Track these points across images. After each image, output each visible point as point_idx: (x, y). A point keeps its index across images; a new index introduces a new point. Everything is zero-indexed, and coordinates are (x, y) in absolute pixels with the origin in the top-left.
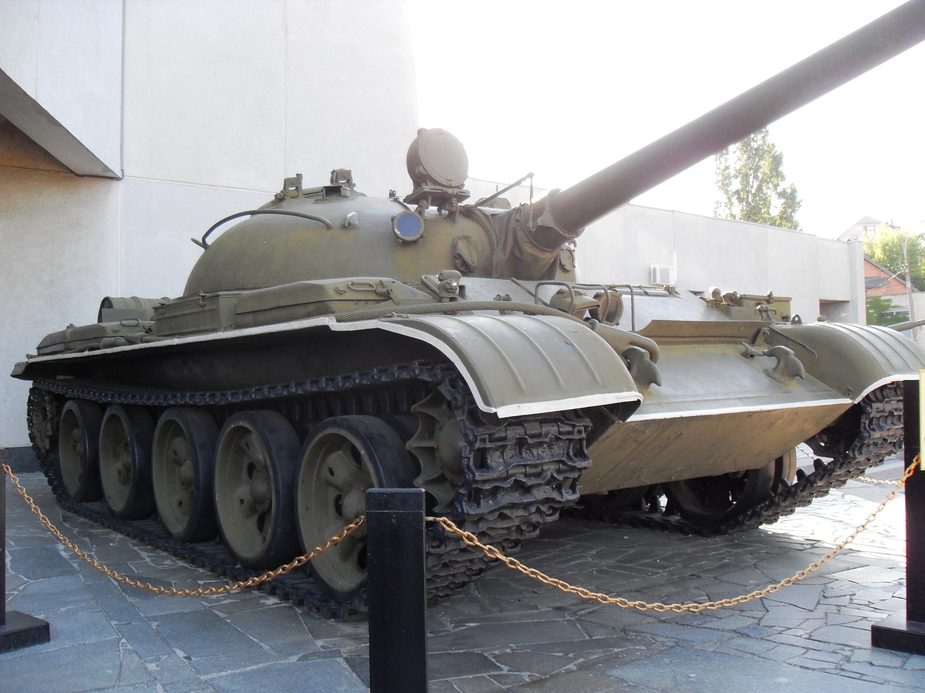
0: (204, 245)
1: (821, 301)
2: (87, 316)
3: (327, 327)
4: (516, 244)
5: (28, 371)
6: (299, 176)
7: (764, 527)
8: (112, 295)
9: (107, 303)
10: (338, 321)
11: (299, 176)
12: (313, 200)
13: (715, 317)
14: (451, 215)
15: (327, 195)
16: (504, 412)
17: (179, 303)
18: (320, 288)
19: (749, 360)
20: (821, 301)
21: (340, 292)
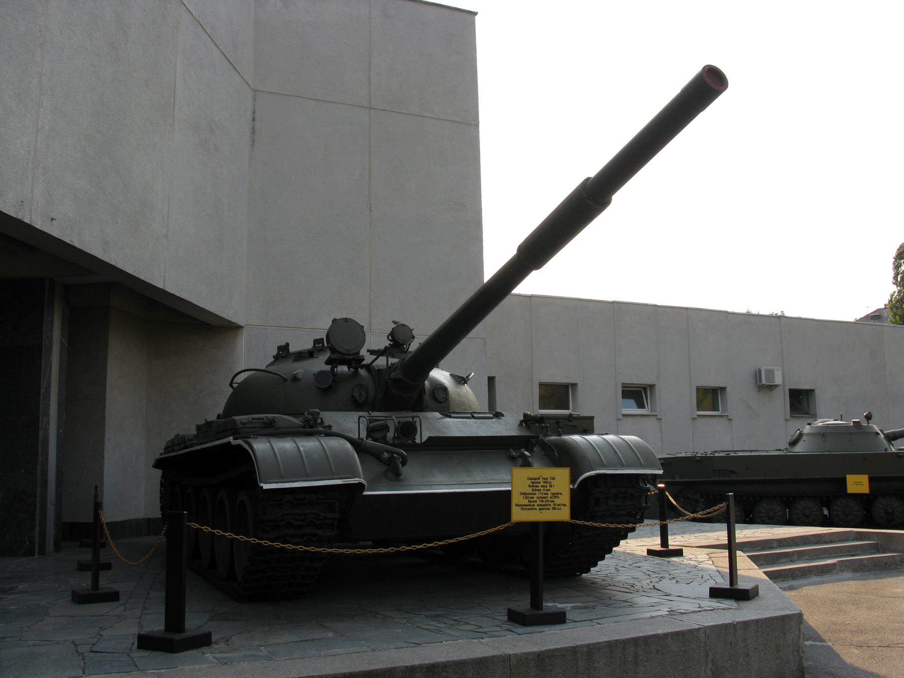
5: (158, 464)
6: (287, 344)
10: (235, 439)
11: (287, 344)
16: (266, 486)
21: (242, 423)
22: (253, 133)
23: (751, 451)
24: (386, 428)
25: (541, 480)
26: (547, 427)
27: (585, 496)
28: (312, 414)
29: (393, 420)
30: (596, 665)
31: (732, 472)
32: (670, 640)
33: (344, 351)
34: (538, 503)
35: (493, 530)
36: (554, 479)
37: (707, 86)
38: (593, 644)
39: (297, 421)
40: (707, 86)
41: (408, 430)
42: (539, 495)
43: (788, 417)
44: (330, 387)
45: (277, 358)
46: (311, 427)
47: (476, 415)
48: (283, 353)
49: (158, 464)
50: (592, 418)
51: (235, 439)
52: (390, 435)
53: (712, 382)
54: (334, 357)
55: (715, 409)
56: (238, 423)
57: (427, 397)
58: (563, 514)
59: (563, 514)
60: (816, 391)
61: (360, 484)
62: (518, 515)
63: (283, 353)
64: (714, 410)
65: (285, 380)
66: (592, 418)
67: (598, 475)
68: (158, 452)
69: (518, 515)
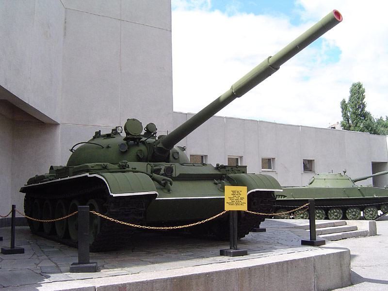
0: (71, 150)
1: (372, 162)
2: (45, 171)
3: (87, 176)
4: (154, 152)
5: (23, 190)
6: (100, 131)
7: (242, 239)
8: (53, 165)
9: (52, 168)
10: (90, 174)
11: (100, 131)
12: (103, 138)
13: (217, 172)
14: (138, 144)
15: (107, 137)
16: (114, 195)
17: (65, 167)
18: (87, 166)
19: (216, 185)
20: (372, 162)
21: (92, 167)
22: (65, 29)
23: (292, 187)
24: (159, 170)
25: (236, 192)
26: (229, 170)
27: (253, 198)
28: (124, 163)
29: (163, 166)
30: (272, 273)
31: (285, 197)
32: (300, 262)
33: (133, 134)
34: (235, 202)
35: (219, 215)
36: (241, 191)
37: (334, 19)
38: (271, 264)
39: (116, 166)
40: (334, 19)
41: (169, 171)
42: (235, 200)
43: (303, 172)
44: (126, 151)
45: (94, 138)
46: (124, 169)
47: (195, 165)
48: (98, 135)
49: (23, 190)
50: (246, 167)
51: (90, 174)
52: (162, 172)
53: (269, 155)
54: (128, 137)
55: (270, 168)
56: (90, 167)
57: (171, 158)
58: (244, 208)
59: (244, 208)
60: (315, 161)
61: (156, 194)
62: (228, 208)
63: (98, 135)
64: (269, 169)
65: (103, 147)
66: (246, 167)
67: (256, 191)
68: (24, 183)
69: (228, 208)
